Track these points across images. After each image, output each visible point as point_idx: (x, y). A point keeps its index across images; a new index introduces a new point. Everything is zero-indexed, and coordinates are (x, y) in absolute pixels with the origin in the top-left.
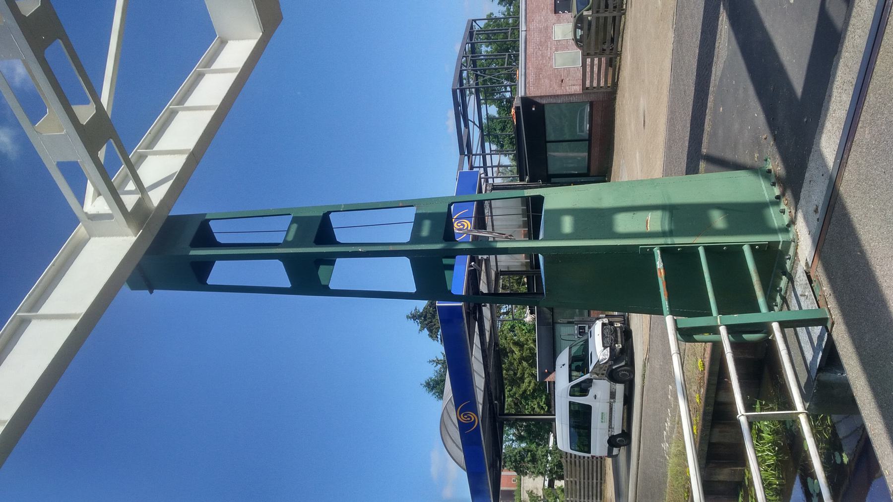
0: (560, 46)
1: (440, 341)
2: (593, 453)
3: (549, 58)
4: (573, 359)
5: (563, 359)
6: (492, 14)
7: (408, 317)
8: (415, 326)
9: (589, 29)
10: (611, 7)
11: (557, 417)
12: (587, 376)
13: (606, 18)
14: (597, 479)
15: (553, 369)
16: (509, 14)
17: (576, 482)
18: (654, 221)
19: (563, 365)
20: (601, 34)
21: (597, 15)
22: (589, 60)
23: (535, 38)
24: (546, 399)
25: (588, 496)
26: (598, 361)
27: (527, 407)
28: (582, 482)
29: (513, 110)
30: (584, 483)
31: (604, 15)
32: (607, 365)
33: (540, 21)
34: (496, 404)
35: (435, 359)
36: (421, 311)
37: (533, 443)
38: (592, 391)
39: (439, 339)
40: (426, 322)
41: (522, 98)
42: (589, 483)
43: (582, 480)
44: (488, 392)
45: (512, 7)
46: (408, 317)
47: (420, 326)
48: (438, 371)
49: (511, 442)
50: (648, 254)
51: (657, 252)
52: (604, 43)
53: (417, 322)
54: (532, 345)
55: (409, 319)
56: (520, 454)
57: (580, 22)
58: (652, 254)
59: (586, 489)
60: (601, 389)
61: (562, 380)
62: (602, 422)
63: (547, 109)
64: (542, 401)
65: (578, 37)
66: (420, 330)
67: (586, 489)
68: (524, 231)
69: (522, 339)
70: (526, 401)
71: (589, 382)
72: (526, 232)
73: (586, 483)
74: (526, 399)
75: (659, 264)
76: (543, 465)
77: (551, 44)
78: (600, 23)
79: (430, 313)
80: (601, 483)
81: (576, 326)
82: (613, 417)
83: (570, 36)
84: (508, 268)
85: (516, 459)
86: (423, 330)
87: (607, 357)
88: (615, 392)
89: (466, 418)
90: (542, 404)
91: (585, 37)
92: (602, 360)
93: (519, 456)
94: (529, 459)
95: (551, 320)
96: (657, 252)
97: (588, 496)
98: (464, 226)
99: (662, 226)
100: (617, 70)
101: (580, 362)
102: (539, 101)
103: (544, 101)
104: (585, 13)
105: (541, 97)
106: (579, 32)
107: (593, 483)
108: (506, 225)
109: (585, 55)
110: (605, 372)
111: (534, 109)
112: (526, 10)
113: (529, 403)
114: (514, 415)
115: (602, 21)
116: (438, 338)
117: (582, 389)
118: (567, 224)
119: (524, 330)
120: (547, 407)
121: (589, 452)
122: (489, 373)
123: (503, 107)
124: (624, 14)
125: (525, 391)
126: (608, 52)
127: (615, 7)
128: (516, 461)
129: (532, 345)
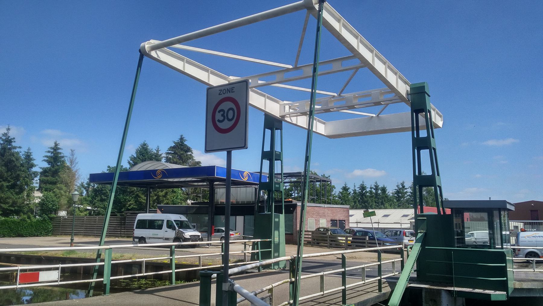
0: (317, 221)
1: (167, 152)
2: (136, 230)
3: (312, 217)
4: (182, 222)
5: (183, 218)
6: (335, 188)
7: (182, 136)
8: (177, 139)
9: (323, 234)
10: (331, 243)
11: (148, 214)
12: (177, 228)
13: (327, 240)
14: (96, 233)
15: (163, 212)
16: (334, 197)
17: (95, 222)
18: (276, 240)
19: (181, 218)
20: (321, 239)
21: (328, 237)
22: (310, 233)
23: (321, 211)
24: (135, 208)
25: (86, 228)
26: (184, 233)
27: (131, 197)
28: (95, 225)
29: (291, 199)
30: (95, 226)
31: (328, 240)
32: (182, 237)
33: (328, 213)
34: (156, 185)
35: (159, 150)
36: (185, 143)
37: (92, 199)
38: (170, 230)
39: (168, 151)
40: (179, 145)
41: (297, 204)
42: (95, 229)
43: (97, 225)
44: (163, 182)
45: (338, 199)
46: (182, 136)
47: (176, 141)
48: (152, 151)
49: (93, 186)
50: (270, 238)
51: (271, 240)
52: (317, 240)
53: (179, 140)
54: (165, 202)
55: (180, 136)
56: (106, 193)
57: (327, 230)
58: (269, 239)
59: (91, 227)
60: (171, 234)
61: (173, 217)
62: (153, 234)
63: (292, 215)
64: (134, 206)
65: (320, 229)
66: (174, 142)
67: (91, 227)
68: (234, 202)
69: (168, 197)
70: (134, 197)
71: (174, 229)
72: (234, 203)
73: (95, 228)
74: (135, 197)
75: (268, 240)
76: (100, 205)
77: (318, 217)
78: (325, 238)
79: (183, 148)
80: (94, 235)
81: (195, 224)
82: (155, 239)
83: (321, 226)
84: (216, 193)
85: (103, 190)
86: (175, 144)
87: (186, 237)
88: (168, 240)
89: (159, 173)
90: (132, 206)
91: (320, 232)
92: (184, 235)
93: (105, 192)
94: (103, 198)
95: (188, 213)
96: (271, 240)
97: (86, 228)
98: (245, 177)
99: (276, 242)
100: (306, 245)
101: (182, 225)
102: (295, 211)
103: (294, 213)
104: (329, 232)
105: (296, 212)
106: (322, 230)
107: (95, 231)
108: (237, 193)
109: (313, 232)
110: (179, 236)
111: (291, 209)
112: (333, 207)
113: (133, 199)
114: (150, 195)
115: (326, 239)
116: (169, 151)
117: (170, 226)
118: (277, 220)
119: (174, 198)
120: (130, 208)
121: (136, 228)
122: (174, 183)
123: (289, 192)
124: (328, 248)
125: (140, 197)
126: (313, 241)
127: (331, 244)
128: (102, 190)
129: (165, 202)
